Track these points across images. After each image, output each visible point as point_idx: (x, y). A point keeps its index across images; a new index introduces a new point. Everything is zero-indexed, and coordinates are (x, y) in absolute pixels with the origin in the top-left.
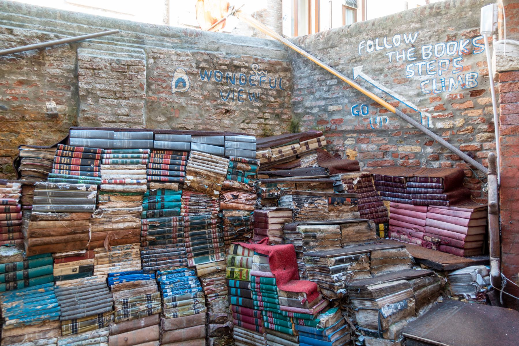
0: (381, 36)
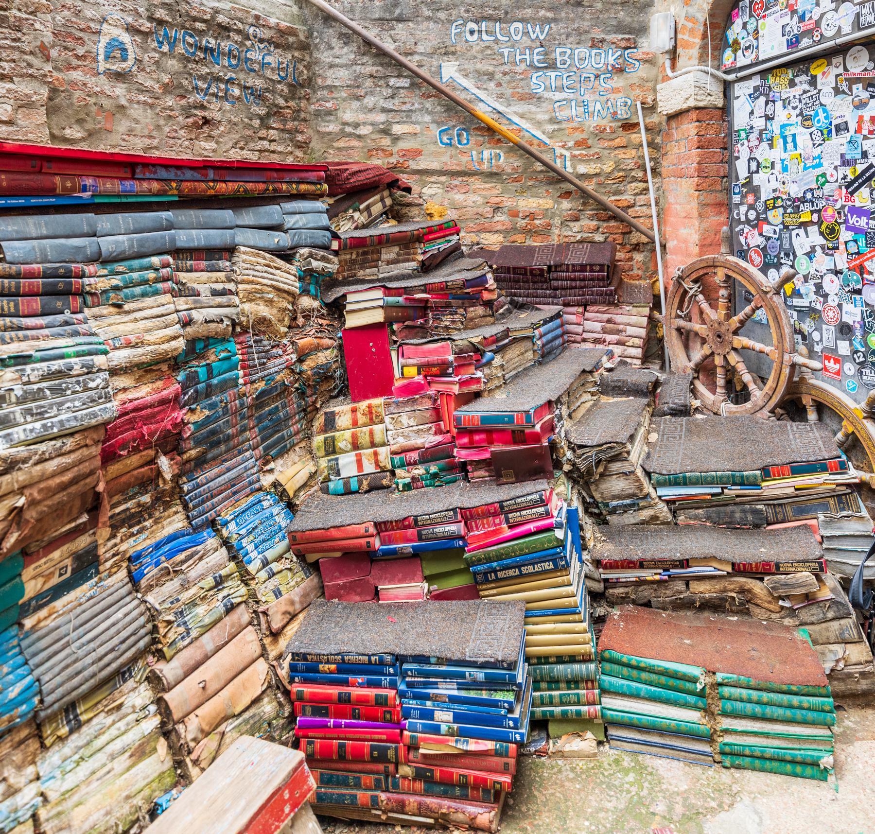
0: (489, 18)
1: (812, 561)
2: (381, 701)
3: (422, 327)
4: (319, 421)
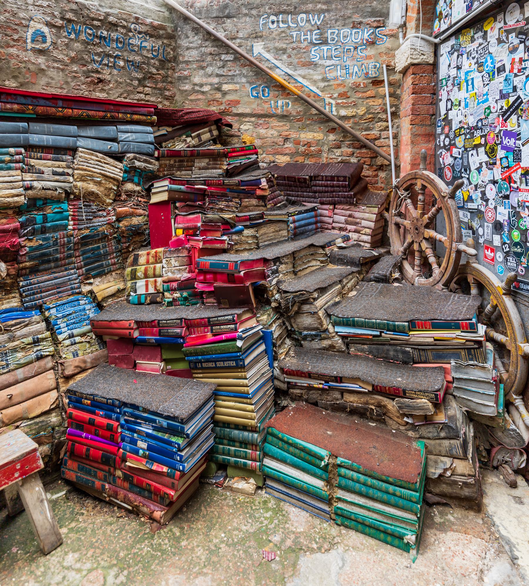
1: (431, 392)
2: (109, 428)
3: (200, 207)
4: (130, 260)
